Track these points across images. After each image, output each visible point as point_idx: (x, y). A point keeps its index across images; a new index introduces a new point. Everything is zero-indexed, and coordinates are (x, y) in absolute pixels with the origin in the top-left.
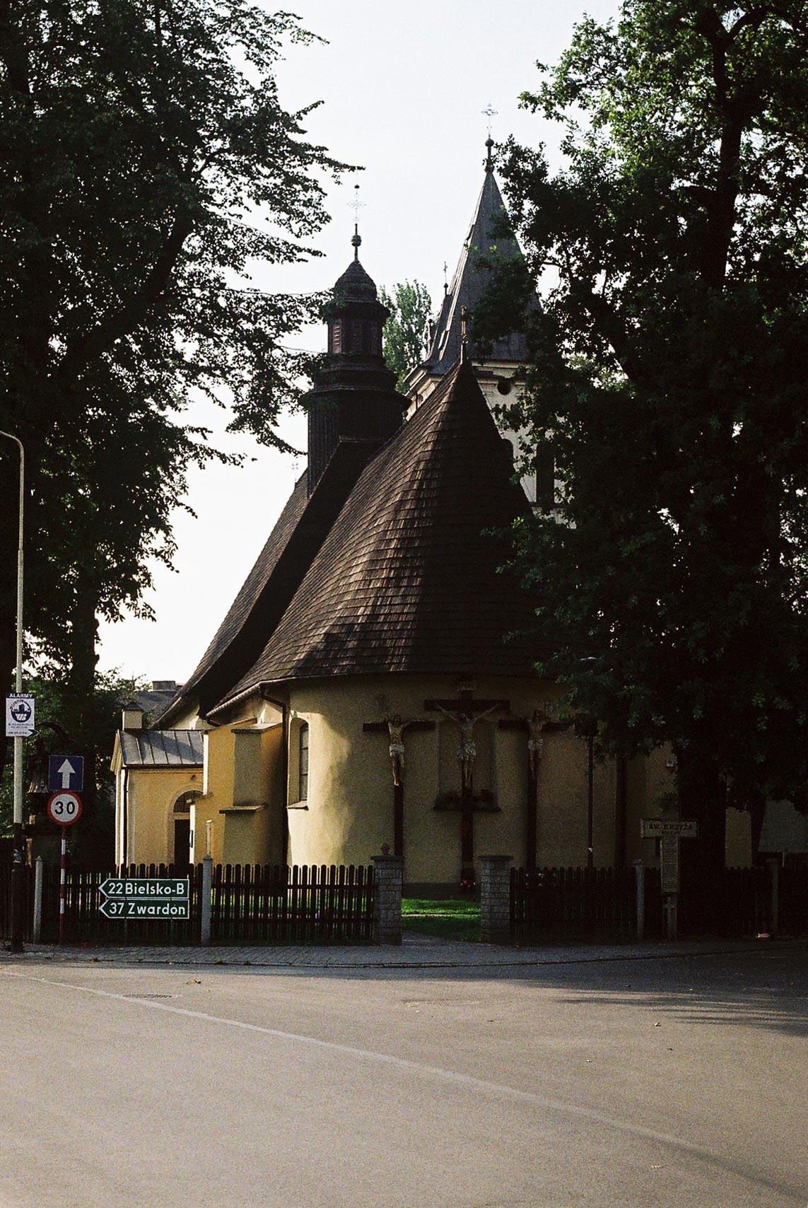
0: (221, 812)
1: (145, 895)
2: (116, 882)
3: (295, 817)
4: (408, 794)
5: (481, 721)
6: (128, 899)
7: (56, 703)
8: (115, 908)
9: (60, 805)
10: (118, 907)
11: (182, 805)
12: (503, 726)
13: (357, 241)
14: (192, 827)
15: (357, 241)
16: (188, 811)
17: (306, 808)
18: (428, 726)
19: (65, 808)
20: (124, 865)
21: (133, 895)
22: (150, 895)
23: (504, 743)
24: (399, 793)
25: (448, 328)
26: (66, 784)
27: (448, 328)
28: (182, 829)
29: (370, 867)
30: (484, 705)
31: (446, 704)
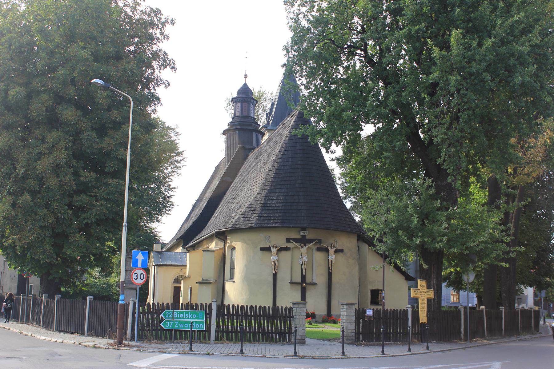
0: (197, 283)
1: (183, 318)
2: (169, 312)
3: (229, 287)
4: (278, 276)
5: (309, 248)
6: (175, 320)
7: (239, 105)
8: (168, 324)
9: (136, 275)
10: (170, 324)
11: (177, 281)
12: (319, 249)
13: (246, 76)
14: (182, 289)
15: (246, 76)
16: (180, 283)
17: (234, 282)
18: (287, 249)
19: (139, 276)
20: (153, 303)
21: (177, 318)
22: (185, 318)
23: (319, 256)
24: (275, 276)
25: (273, 113)
26: (140, 264)
27: (273, 113)
28: (177, 291)
29: (291, 307)
30: (310, 241)
31: (296, 240)
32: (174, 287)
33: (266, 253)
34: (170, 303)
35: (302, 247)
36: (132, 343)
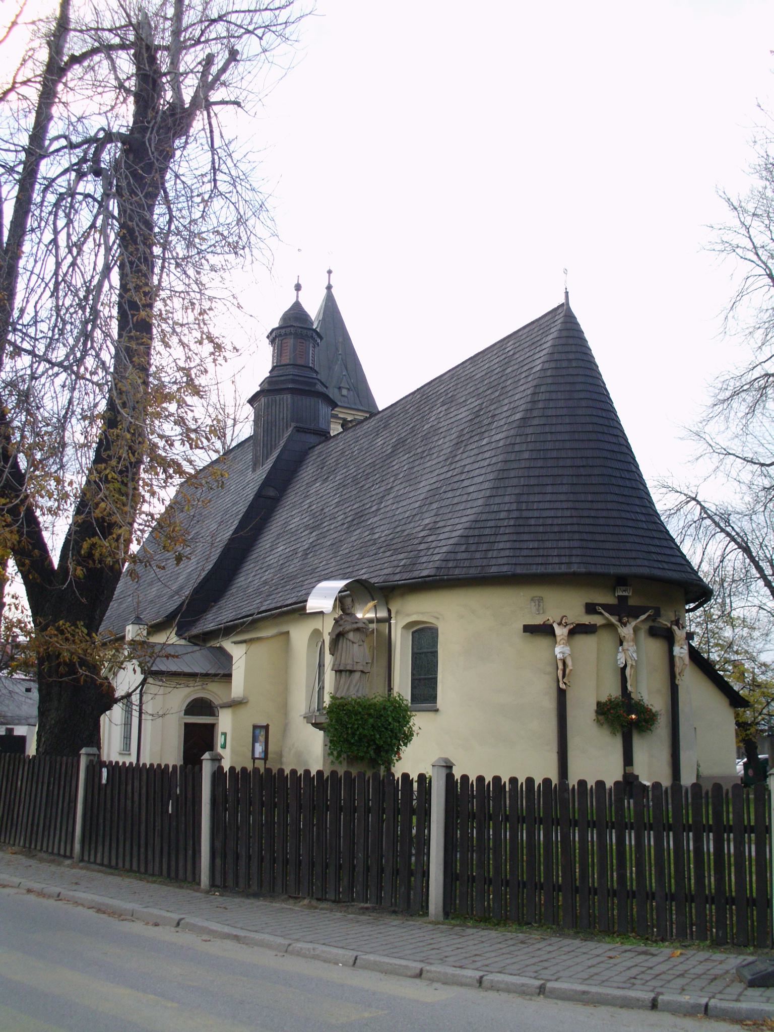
13: (298, 288)
15: (298, 288)
31: (608, 608)
32: (186, 725)
33: (542, 642)
34: (609, 784)
35: (624, 624)
36: (329, 676)
